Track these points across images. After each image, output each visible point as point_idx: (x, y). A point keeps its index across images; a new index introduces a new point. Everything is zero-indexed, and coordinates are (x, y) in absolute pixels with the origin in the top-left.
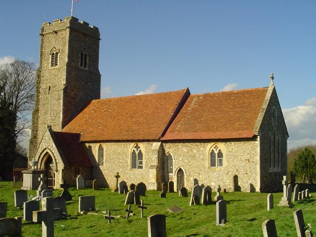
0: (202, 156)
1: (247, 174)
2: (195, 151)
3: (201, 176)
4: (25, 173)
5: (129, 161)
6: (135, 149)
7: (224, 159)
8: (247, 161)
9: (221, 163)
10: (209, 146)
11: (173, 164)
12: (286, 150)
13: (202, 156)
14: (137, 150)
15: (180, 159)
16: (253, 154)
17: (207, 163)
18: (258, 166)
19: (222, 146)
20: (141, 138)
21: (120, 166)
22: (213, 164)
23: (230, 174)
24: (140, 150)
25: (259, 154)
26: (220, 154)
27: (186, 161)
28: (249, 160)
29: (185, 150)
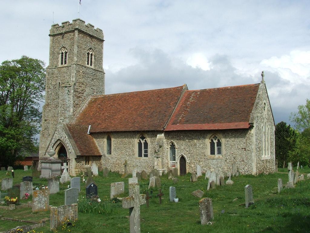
0: (202, 145)
1: (243, 161)
3: (201, 163)
8: (244, 149)
16: (249, 143)
19: (219, 136)
20: (146, 129)
22: (212, 152)
24: (145, 140)
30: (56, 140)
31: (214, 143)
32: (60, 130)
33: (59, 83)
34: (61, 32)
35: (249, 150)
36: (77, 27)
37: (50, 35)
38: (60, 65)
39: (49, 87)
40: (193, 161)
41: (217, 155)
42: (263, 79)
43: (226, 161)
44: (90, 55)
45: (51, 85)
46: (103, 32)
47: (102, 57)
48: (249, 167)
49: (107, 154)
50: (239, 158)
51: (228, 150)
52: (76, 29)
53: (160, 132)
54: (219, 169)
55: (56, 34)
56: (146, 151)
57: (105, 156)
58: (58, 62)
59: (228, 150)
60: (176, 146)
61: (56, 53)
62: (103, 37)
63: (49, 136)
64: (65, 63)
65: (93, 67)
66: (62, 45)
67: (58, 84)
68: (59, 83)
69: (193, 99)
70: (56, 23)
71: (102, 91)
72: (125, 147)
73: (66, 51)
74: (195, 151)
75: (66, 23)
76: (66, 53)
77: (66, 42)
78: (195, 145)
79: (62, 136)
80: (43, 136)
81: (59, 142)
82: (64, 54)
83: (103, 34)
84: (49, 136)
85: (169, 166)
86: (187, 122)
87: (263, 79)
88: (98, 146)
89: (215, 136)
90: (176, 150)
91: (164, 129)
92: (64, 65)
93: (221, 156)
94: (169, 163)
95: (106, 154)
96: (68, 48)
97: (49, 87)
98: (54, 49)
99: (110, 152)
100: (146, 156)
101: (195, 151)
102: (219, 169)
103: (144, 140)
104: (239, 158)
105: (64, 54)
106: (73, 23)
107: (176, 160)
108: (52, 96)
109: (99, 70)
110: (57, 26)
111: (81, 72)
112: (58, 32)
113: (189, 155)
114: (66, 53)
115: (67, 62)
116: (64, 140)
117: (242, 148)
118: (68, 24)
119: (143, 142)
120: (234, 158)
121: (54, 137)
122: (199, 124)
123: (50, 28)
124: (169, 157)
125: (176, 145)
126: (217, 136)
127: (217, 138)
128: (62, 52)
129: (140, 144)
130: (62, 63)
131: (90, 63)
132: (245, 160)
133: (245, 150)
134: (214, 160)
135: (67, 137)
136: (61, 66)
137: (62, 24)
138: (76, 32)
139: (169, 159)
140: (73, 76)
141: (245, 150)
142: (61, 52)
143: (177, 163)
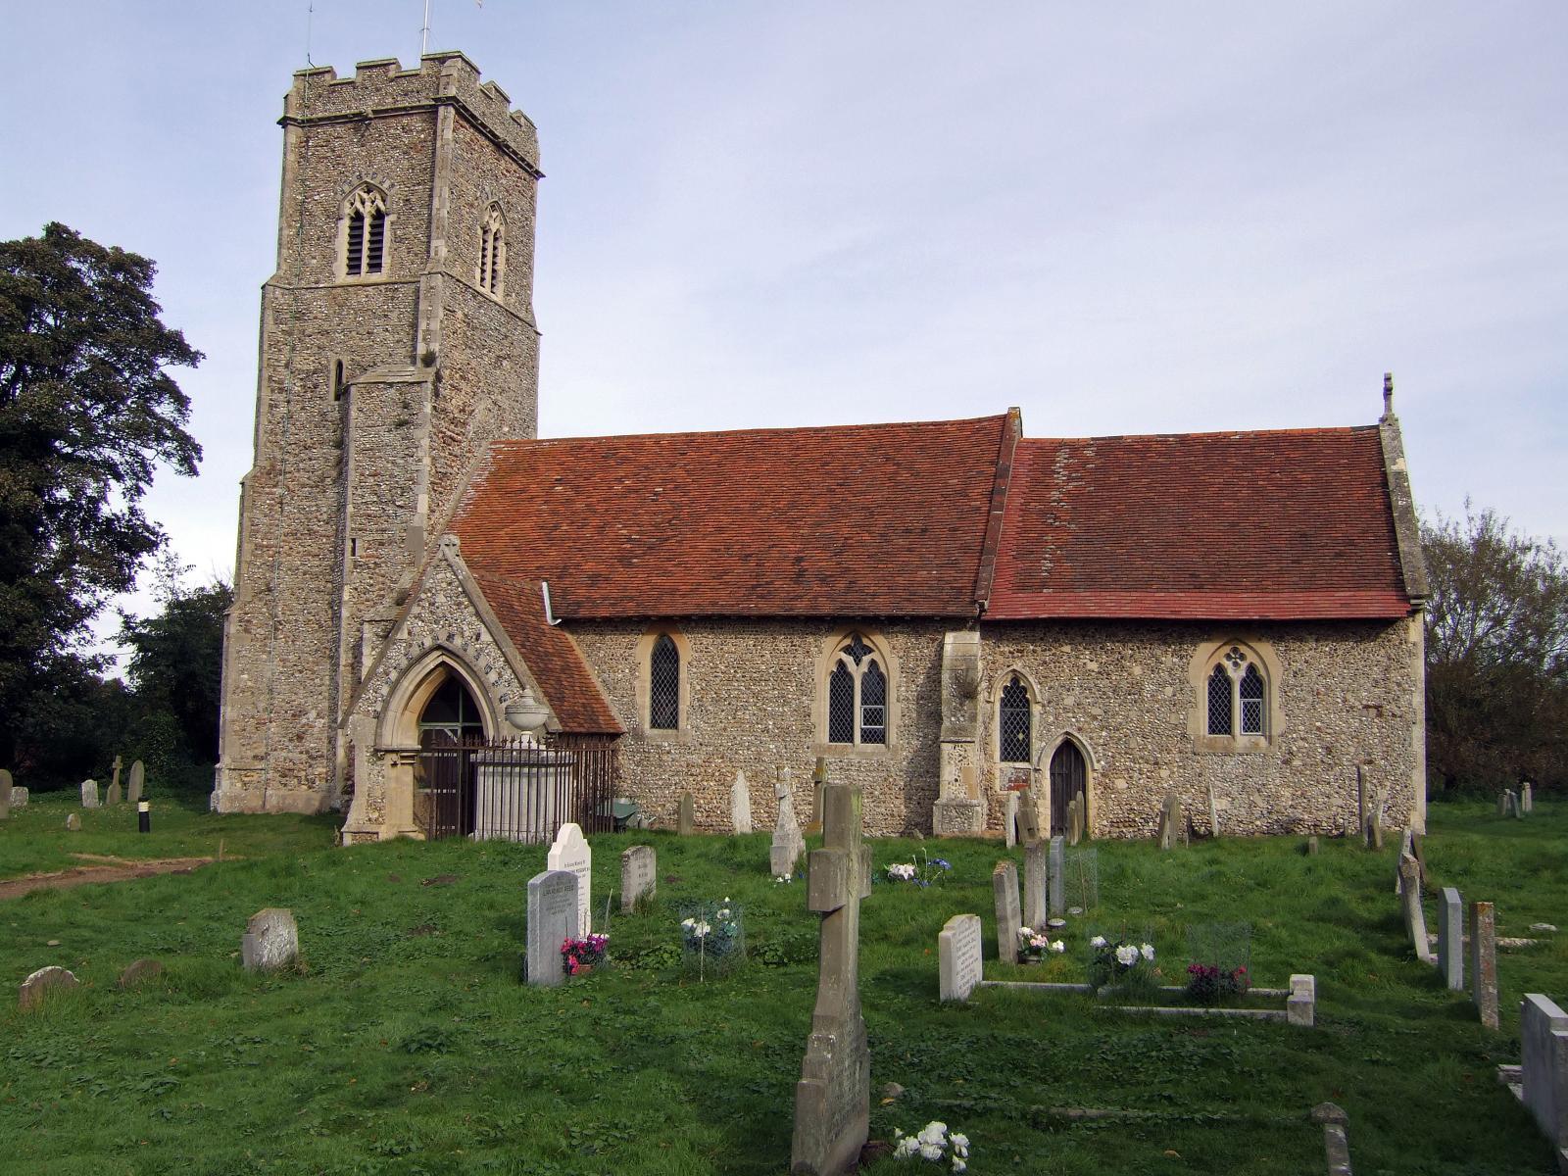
0: (1169, 691)
1: (1370, 762)
2: (1137, 670)
3: (1164, 773)
4: (485, 764)
5: (821, 708)
6: (849, 660)
7: (1275, 697)
8: (1373, 712)
9: (1254, 721)
10: (1204, 657)
11: (1035, 721)
12: (1531, 992)
13: (1169, 691)
14: (858, 662)
15: (1069, 701)
16: (1399, 685)
17: (1200, 718)
18: (1419, 733)
19: (1267, 655)
20: (881, 607)
21: (766, 730)
22: (1220, 722)
23: (1297, 763)
24: (873, 663)
25: (1422, 685)
26: (1254, 685)
27: (1096, 711)
28: (1377, 707)
29: (1094, 666)
30: (415, 651)
31: (1228, 682)
32: (441, 599)
33: (340, 365)
34: (349, 108)
35: (1398, 713)
36: (452, 91)
37: (284, 122)
38: (342, 276)
39: (281, 382)
40: (1123, 762)
41: (1241, 738)
42: (1388, 408)
43: (1286, 762)
44: (490, 239)
45: (286, 372)
46: (540, 135)
47: (530, 256)
48: (1398, 788)
49: (655, 724)
50: (1352, 749)
51: (1297, 711)
52: (452, 101)
53: (957, 623)
54: (1256, 798)
55: (320, 119)
56: (874, 717)
57: (638, 735)
58: (329, 259)
59: (1297, 711)
60: (1037, 691)
61: (318, 211)
62: (536, 159)
63: (276, 629)
64: (375, 266)
65: (498, 298)
66: (360, 177)
67: (333, 367)
68: (340, 365)
69: (1070, 479)
70: (320, 63)
71: (530, 420)
72: (755, 695)
73: (383, 208)
74: (1133, 715)
75: (384, 65)
76: (379, 216)
77: (386, 161)
78: (1136, 688)
79: (453, 629)
80: (247, 631)
81: (432, 661)
82: (367, 221)
83: (536, 141)
84: (276, 629)
85: (997, 788)
86: (1092, 582)
87: (1388, 408)
88: (600, 686)
89: (1235, 650)
90: (1036, 709)
91: (983, 610)
92: (365, 276)
93: (1263, 742)
94: (997, 774)
95: (647, 725)
96: (393, 191)
97: (281, 382)
98: (308, 193)
99: (665, 713)
100: (874, 736)
101: (1133, 715)
102: (1256, 798)
103: (866, 659)
104: (1352, 749)
105: (367, 221)
106: (424, 72)
107: (1035, 759)
108: (293, 429)
109: (521, 316)
110: (327, 77)
111: (459, 314)
112: (332, 110)
113: (1104, 734)
114: (379, 216)
115: (386, 260)
116: (471, 651)
117: (1367, 707)
118: (392, 74)
119: (858, 672)
120: (1329, 750)
121: (405, 635)
122: (1159, 590)
123: (288, 85)
124: (998, 744)
125: (1037, 688)
126: (1243, 649)
127: (1243, 657)
128: (357, 213)
129: (841, 679)
130: (354, 266)
131: (488, 275)
132: (1377, 754)
133: (1377, 716)
134: (1227, 759)
135: (486, 637)
136: (352, 279)
137: (358, 68)
138: (447, 114)
139: (997, 755)
140: (428, 331)
141: (1377, 716)
142: (348, 210)
143: (1036, 770)
